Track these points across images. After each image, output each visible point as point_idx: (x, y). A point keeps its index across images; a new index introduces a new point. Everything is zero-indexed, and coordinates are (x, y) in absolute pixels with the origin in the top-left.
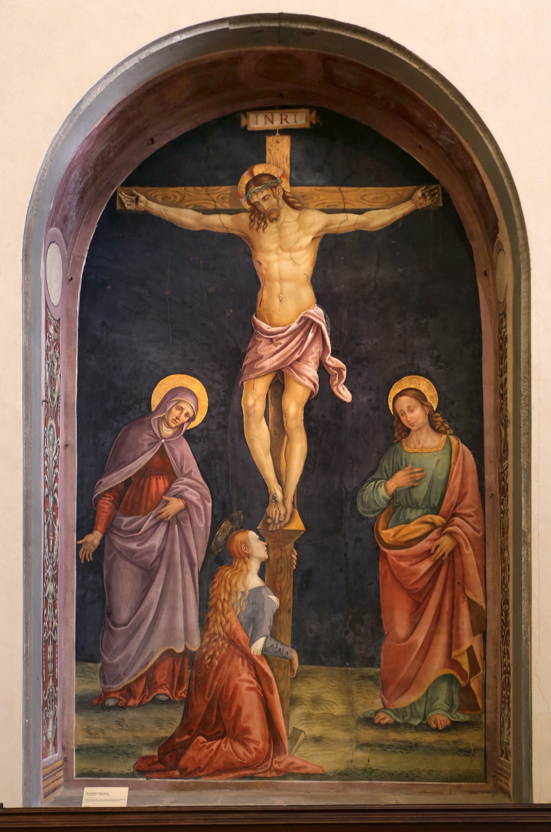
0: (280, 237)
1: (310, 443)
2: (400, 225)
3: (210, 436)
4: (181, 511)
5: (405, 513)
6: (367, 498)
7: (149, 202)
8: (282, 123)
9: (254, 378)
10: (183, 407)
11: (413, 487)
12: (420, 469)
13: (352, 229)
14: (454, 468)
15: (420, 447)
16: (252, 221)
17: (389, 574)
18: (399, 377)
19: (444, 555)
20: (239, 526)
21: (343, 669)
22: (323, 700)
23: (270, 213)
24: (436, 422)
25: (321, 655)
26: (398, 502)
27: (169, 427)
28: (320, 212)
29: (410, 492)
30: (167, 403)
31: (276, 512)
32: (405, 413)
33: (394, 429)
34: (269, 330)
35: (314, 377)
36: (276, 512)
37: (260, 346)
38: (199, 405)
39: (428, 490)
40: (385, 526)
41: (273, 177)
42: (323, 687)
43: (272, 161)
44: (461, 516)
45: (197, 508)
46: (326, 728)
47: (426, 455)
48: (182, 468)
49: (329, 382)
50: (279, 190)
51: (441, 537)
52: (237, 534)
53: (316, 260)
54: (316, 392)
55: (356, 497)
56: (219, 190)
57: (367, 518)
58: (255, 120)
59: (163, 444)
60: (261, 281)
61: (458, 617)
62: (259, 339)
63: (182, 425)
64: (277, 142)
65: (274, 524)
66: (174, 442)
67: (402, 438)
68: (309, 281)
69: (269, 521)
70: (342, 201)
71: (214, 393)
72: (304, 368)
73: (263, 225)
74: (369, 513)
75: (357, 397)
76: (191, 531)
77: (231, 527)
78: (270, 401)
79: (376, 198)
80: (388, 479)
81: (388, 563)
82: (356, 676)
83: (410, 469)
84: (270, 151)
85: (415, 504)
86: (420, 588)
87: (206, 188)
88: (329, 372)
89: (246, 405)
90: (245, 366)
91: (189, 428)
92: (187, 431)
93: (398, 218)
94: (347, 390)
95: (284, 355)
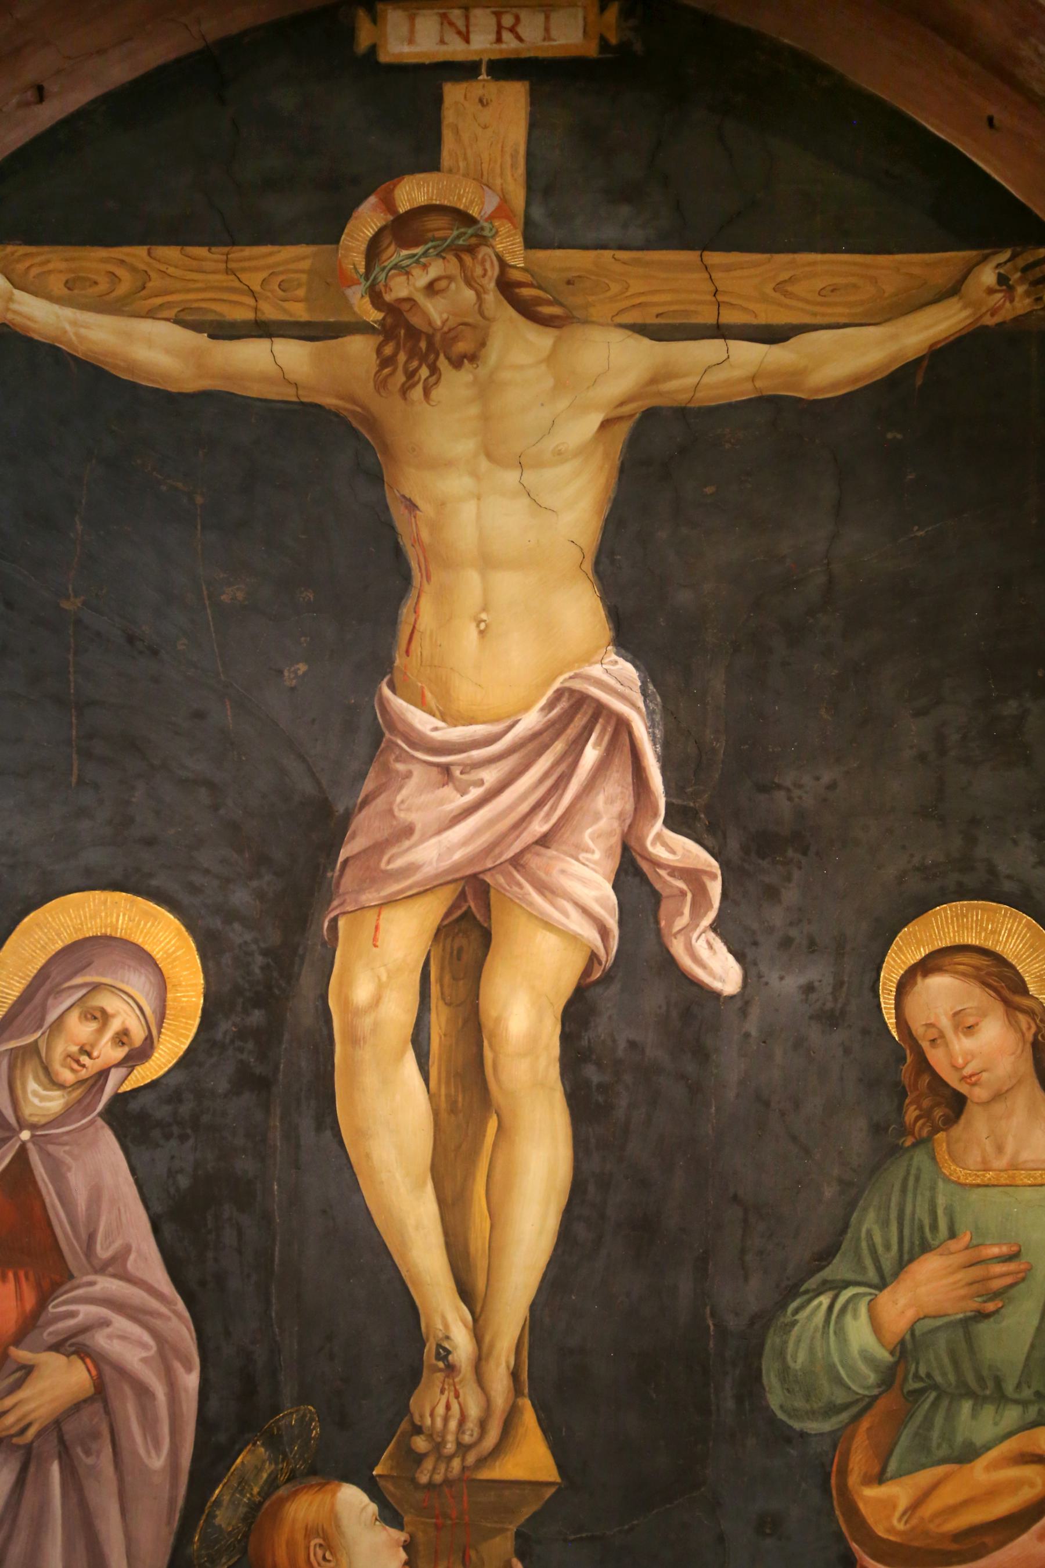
0: (485, 418)
1: (581, 1146)
2: (919, 382)
3: (205, 1119)
4: (76, 1407)
5: (951, 1417)
6: (802, 1356)
7: (16, 292)
8: (499, 40)
9: (380, 906)
10: (110, 1010)
11: (981, 1316)
12: (1005, 1249)
13: (746, 392)
15: (1002, 1162)
16: (386, 362)
18: (922, 906)
20: (301, 1466)
23: (451, 337)
26: (922, 1372)
27: (53, 1082)
28: (630, 333)
29: (969, 1339)
30: (48, 994)
31: (448, 1407)
32: (942, 1035)
33: (903, 1094)
34: (437, 735)
35: (601, 901)
36: (448, 1407)
37: (404, 792)
38: (170, 1003)
40: (877, 1469)
41: (465, 219)
43: (462, 164)
45: (143, 1392)
47: (1028, 1194)
48: (92, 1237)
49: (657, 922)
50: (483, 261)
52: (295, 1494)
53: (613, 496)
54: (608, 954)
55: (760, 1355)
56: (271, 260)
57: (803, 1435)
58: (404, 30)
59: (23, 1148)
60: (414, 565)
62: (400, 767)
63: (103, 1075)
64: (481, 101)
65: (440, 1457)
66: (65, 1138)
67: (936, 1130)
68: (588, 566)
69: (420, 1444)
70: (709, 298)
71: (227, 959)
72: (563, 872)
73: (423, 377)
74: (812, 1414)
75: (760, 976)
76: (113, 1487)
77: (268, 1468)
78: (435, 989)
79: (833, 291)
80: (882, 1285)
83: (967, 1248)
84: (457, 132)
85: (990, 1384)
87: (226, 249)
88: (658, 886)
89: (346, 1003)
90: (346, 862)
91: (126, 1087)
92: (120, 1099)
93: (911, 356)
94: (724, 949)
95: (491, 823)
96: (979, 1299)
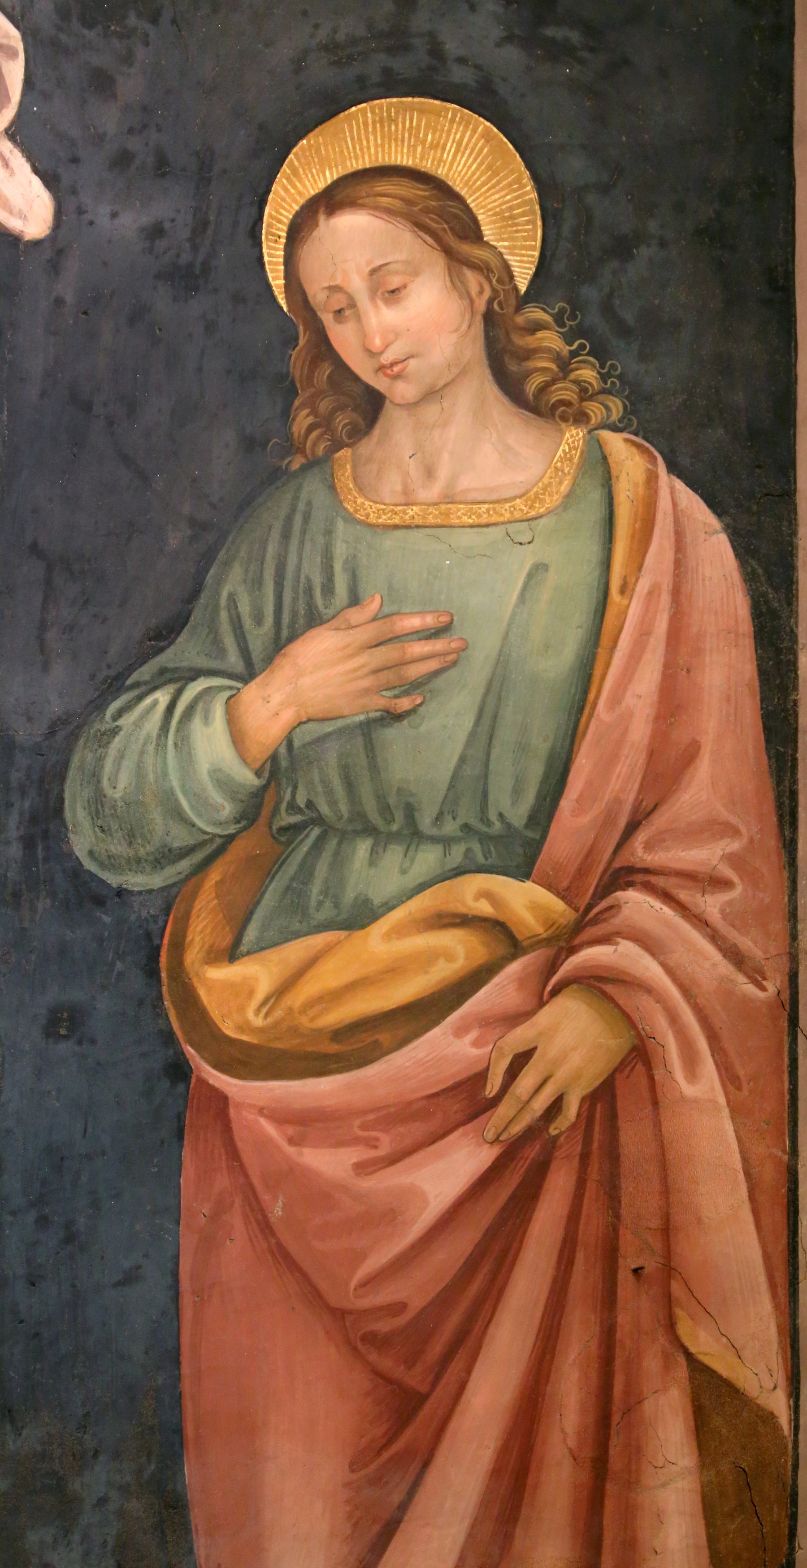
5: (339, 862)
6: (124, 780)
11: (392, 717)
12: (429, 620)
14: (624, 613)
15: (433, 492)
17: (236, 1219)
19: (556, 1107)
24: (529, 354)
26: (301, 801)
29: (370, 748)
32: (353, 305)
33: (292, 392)
39: (473, 735)
40: (227, 940)
44: (660, 881)
51: (541, 1004)
55: (61, 777)
57: (120, 892)
67: (337, 445)
80: (249, 674)
81: (234, 1154)
85: (399, 816)
86: (417, 1303)
94: (27, 168)
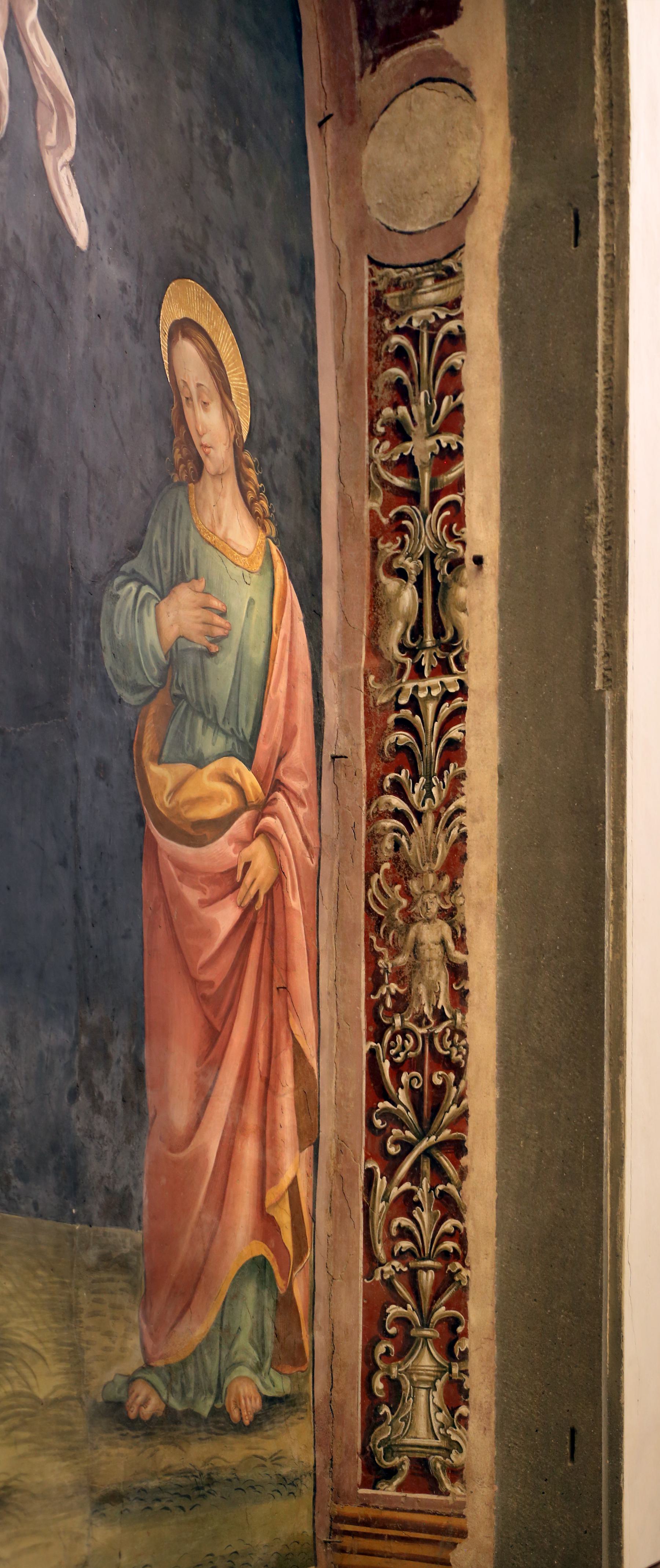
19: (257, 895)
21: (64, 1227)
22: (12, 1344)
25: (11, 1171)
42: (11, 1296)
46: (22, 1449)
61: (275, 1093)
82: (91, 1256)
96: (209, 639)
